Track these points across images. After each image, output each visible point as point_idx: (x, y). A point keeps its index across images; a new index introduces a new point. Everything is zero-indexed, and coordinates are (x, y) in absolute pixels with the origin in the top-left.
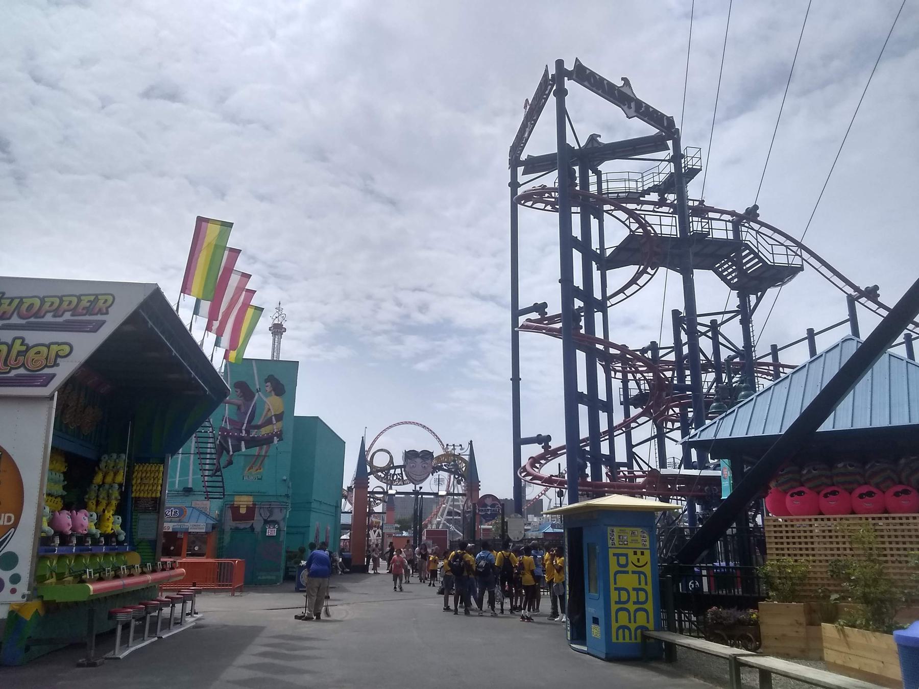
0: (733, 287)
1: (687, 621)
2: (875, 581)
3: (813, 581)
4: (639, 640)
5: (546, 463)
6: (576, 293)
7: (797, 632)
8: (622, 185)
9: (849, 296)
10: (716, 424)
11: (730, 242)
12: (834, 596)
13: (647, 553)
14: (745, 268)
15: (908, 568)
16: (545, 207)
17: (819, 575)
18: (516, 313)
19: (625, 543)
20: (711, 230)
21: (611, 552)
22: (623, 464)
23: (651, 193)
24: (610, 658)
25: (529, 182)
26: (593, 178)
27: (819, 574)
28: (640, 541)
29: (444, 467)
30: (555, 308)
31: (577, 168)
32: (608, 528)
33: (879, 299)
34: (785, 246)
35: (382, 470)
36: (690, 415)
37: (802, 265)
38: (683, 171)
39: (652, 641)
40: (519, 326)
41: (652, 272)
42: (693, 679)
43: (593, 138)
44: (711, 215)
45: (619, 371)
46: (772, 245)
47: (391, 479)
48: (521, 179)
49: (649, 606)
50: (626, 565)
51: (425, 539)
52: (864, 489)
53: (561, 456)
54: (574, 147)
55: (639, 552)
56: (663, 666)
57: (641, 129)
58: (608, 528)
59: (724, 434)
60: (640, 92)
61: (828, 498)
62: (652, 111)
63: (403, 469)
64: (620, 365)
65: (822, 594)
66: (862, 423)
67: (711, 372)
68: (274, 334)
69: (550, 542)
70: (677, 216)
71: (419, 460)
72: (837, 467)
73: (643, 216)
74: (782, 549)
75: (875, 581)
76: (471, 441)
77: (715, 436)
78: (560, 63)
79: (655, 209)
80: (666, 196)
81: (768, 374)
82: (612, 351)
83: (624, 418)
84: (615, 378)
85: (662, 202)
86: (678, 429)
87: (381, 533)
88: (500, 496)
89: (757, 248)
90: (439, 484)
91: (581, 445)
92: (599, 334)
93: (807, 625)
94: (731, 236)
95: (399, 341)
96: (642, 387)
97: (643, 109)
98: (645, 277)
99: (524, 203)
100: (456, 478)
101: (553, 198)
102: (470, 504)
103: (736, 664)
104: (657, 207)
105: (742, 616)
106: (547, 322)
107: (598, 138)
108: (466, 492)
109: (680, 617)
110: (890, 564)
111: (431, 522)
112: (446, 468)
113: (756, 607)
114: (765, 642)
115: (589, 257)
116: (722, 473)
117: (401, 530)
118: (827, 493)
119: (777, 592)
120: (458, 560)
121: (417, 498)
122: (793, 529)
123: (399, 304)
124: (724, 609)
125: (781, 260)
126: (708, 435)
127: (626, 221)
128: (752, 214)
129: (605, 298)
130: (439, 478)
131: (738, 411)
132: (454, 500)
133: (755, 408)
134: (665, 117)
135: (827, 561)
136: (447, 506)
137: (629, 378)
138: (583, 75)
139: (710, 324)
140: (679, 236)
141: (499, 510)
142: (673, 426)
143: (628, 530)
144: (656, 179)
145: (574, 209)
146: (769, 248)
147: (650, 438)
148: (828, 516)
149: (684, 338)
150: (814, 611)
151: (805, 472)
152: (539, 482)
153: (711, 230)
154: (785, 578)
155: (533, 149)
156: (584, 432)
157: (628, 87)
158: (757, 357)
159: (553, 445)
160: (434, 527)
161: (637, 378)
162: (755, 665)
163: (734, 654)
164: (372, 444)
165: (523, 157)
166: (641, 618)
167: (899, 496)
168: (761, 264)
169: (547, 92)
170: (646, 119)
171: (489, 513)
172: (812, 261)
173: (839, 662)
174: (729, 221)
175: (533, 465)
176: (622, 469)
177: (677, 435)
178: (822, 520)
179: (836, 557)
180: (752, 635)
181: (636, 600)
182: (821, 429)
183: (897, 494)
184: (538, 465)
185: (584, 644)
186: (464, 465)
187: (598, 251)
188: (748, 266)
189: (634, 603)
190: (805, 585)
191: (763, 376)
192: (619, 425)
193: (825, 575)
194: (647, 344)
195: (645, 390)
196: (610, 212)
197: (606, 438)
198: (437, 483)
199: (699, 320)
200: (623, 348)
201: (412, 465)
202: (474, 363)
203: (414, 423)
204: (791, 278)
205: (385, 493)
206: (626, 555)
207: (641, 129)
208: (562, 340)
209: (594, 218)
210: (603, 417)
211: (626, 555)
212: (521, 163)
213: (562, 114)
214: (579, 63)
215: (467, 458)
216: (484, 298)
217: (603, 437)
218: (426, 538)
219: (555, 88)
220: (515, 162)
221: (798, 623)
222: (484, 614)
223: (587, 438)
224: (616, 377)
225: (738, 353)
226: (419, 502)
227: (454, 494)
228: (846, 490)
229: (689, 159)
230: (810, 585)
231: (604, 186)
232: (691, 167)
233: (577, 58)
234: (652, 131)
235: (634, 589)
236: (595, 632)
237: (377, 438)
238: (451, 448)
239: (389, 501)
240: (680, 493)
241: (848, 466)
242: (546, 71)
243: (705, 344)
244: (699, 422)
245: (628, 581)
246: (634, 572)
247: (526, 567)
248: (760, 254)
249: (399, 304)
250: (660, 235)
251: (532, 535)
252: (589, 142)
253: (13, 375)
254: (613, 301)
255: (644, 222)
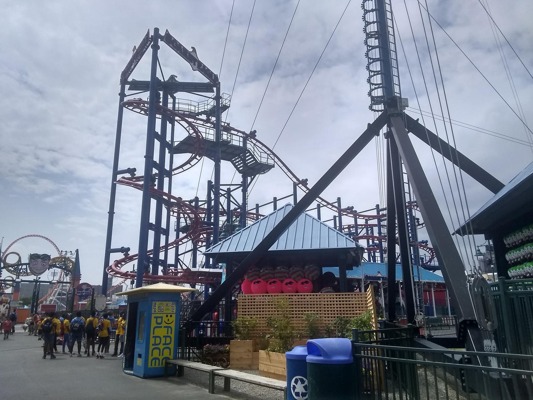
0: (240, 172)
1: (197, 353)
2: (286, 327)
3: (259, 328)
4: (164, 365)
5: (125, 264)
6: (155, 165)
7: (248, 356)
8: (187, 107)
9: (294, 183)
10: (221, 245)
11: (241, 148)
12: (267, 336)
13: (174, 316)
14: (247, 162)
15: (302, 321)
16: (140, 112)
17: (262, 325)
18: (116, 172)
19: (162, 310)
20: (231, 140)
21: (153, 316)
22: (172, 265)
23: (202, 115)
24: (146, 377)
25: (132, 95)
26: (170, 100)
27: (262, 324)
28: (170, 309)
29: (58, 265)
30: (140, 172)
31: (161, 93)
32: (153, 302)
33: (308, 186)
34: (267, 154)
35: (12, 266)
36: (212, 238)
37: (274, 165)
38: (220, 106)
39: (172, 365)
40: (117, 180)
41: (199, 158)
42: (191, 385)
43: (172, 77)
44: (232, 132)
45: (176, 212)
46: (261, 152)
47: (19, 272)
48: (127, 92)
49: (172, 346)
50: (161, 323)
51: (40, 310)
52: (288, 281)
53: (135, 260)
54: (161, 80)
55: (169, 315)
56: (176, 379)
57: (200, 78)
58: (153, 302)
59: (224, 250)
60: (201, 57)
61: (271, 285)
62: (207, 69)
63: (28, 266)
64: (177, 208)
65: (262, 335)
66: (290, 247)
67: (225, 216)
69: (120, 312)
70: (215, 130)
71: (40, 260)
72: (277, 269)
73: (197, 127)
74: (245, 312)
75: (286, 327)
77: (219, 251)
78: (156, 30)
79: (204, 124)
80: (210, 117)
81: (253, 219)
82: (172, 200)
83: (175, 239)
84: (173, 216)
85: (208, 121)
86: (204, 246)
87: (8, 307)
88: (92, 283)
89: (254, 153)
90: (54, 276)
91: (148, 254)
92: (166, 190)
93: (253, 352)
94: (241, 145)
95: (34, 182)
96: (188, 222)
97: (202, 67)
98: (195, 161)
99: (128, 107)
100: (65, 272)
101: (146, 107)
102: (71, 288)
103: (213, 374)
104: (205, 123)
105: (221, 348)
106: (135, 180)
107: (176, 78)
108: (71, 281)
109: (189, 351)
110: (295, 319)
111: (46, 300)
112: (58, 266)
113: (229, 343)
114: (231, 362)
115: (164, 145)
116: (223, 271)
117: (23, 304)
118: (303, 282)
119: (240, 335)
120: (48, 323)
121: (36, 284)
122: (254, 301)
123: (37, 158)
124: (213, 345)
125: (264, 161)
126: (216, 250)
127: (187, 128)
128: (253, 135)
129: (171, 170)
130: (54, 272)
131: (233, 238)
132: (63, 286)
134: (213, 74)
135: (266, 318)
136: (58, 290)
137: (181, 216)
138: (169, 40)
139: (227, 190)
140: (215, 141)
141: (91, 292)
142: (202, 245)
143: (165, 303)
144: (206, 107)
145: (157, 116)
146: (259, 153)
147: (191, 250)
148: (301, 294)
149: (213, 196)
150: (258, 344)
151: (261, 271)
152: (119, 275)
153: (231, 140)
154: (245, 327)
155: (134, 76)
156: (150, 246)
157: (195, 53)
158: (248, 210)
159: (131, 253)
160: (48, 303)
161: (186, 217)
162: (222, 375)
163: (212, 370)
164: (8, 248)
165: (130, 79)
166: (166, 353)
167: (271, 284)
168: (255, 161)
169: (147, 45)
170: (203, 73)
172: (279, 163)
173: (266, 370)
174: (241, 137)
175: (116, 265)
176: (171, 268)
177: (203, 249)
178: (269, 296)
179: (270, 316)
180: (226, 359)
181: (164, 343)
182: (271, 249)
183: (302, 283)
184: (119, 265)
185: (132, 370)
186: (71, 264)
187: (170, 143)
188: (248, 161)
189: (163, 344)
190: (254, 330)
191: (251, 220)
192: (172, 243)
193: (264, 325)
194: (193, 198)
195: (189, 223)
196: (179, 121)
197: (163, 250)
198: (53, 275)
199: (221, 187)
200: (178, 200)
201: (34, 263)
202: (86, 200)
203: (40, 236)
204: (268, 171)
205: (13, 281)
206: (162, 317)
207: (200, 78)
208: (142, 191)
209: (169, 123)
210: (163, 238)
211: (162, 317)
212: (128, 83)
213: (155, 59)
214: (168, 33)
215: (74, 260)
216: (97, 161)
217: (162, 250)
218: (41, 309)
219: (152, 43)
220: (124, 81)
221: (248, 351)
222: (73, 356)
223: (152, 250)
224: (174, 215)
225: (239, 207)
226: (37, 288)
227: (63, 282)
228: (280, 281)
229: (224, 100)
230: (257, 330)
231: (177, 106)
232: (225, 104)
233: (167, 30)
234: (206, 80)
235: (164, 337)
236: (139, 362)
237: (12, 244)
238: (64, 253)
239: (16, 286)
240: (201, 281)
241: (282, 269)
242: (148, 33)
243: (223, 200)
244: (215, 241)
245: (161, 332)
246: (165, 327)
247: (106, 326)
248: (255, 156)
249: (37, 158)
250: (205, 139)
251: (112, 307)
252: (170, 79)
254: (176, 172)
255: (197, 130)
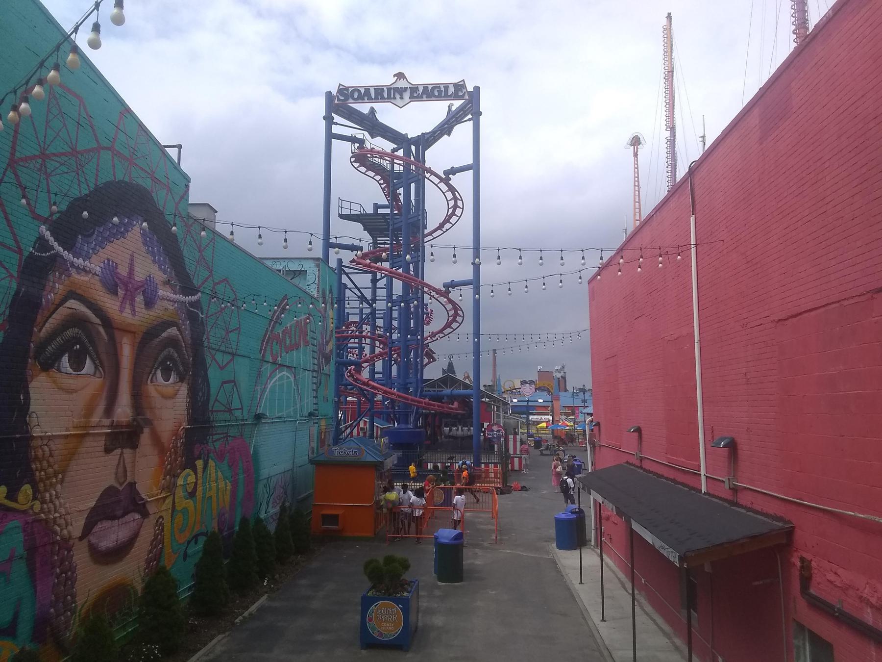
68: (175, 224)
71: (527, 385)
76: (669, 14)
133: (703, 129)
171: (495, 436)
253: (98, 320)
